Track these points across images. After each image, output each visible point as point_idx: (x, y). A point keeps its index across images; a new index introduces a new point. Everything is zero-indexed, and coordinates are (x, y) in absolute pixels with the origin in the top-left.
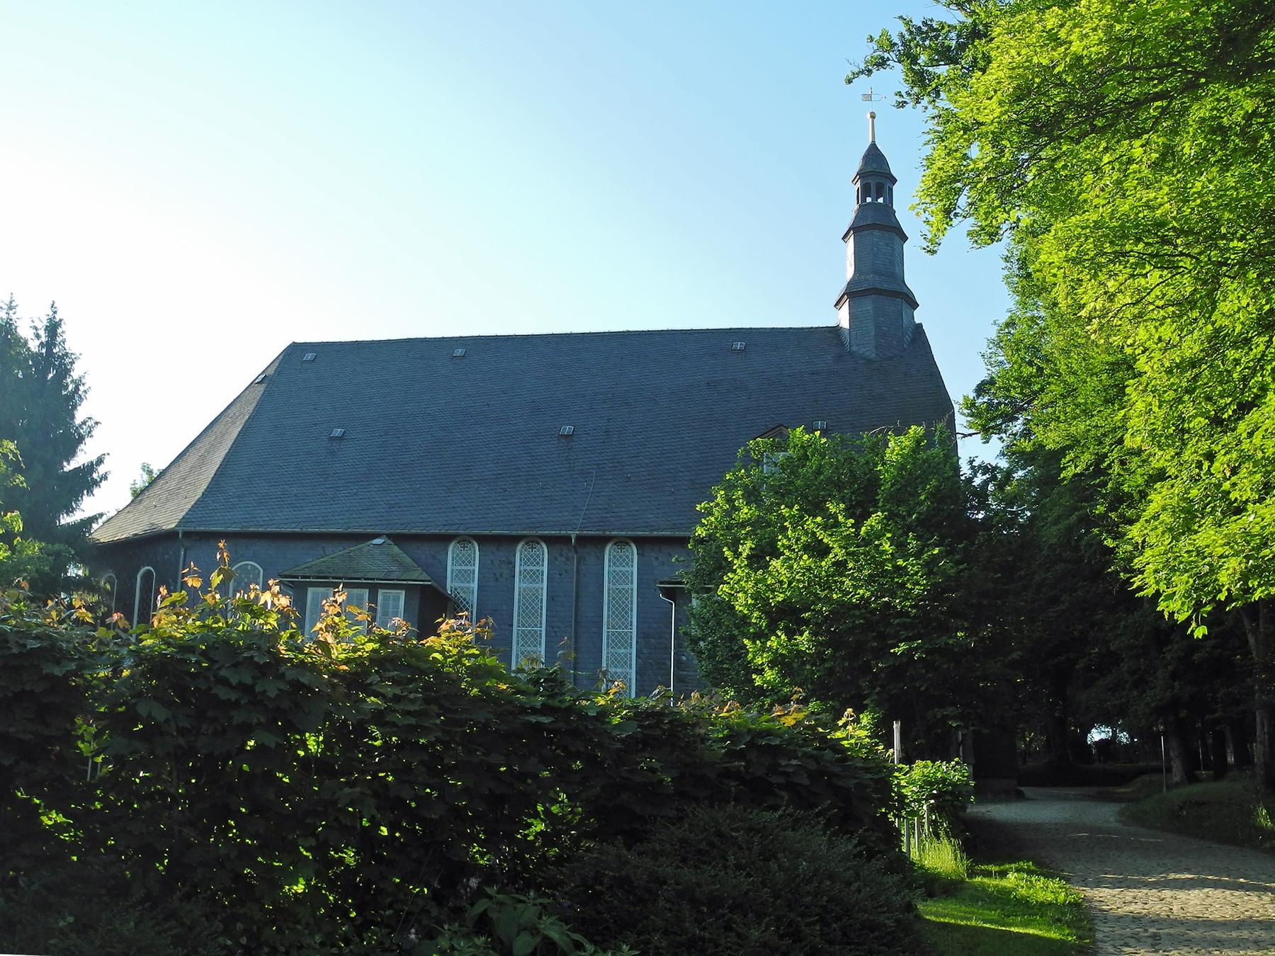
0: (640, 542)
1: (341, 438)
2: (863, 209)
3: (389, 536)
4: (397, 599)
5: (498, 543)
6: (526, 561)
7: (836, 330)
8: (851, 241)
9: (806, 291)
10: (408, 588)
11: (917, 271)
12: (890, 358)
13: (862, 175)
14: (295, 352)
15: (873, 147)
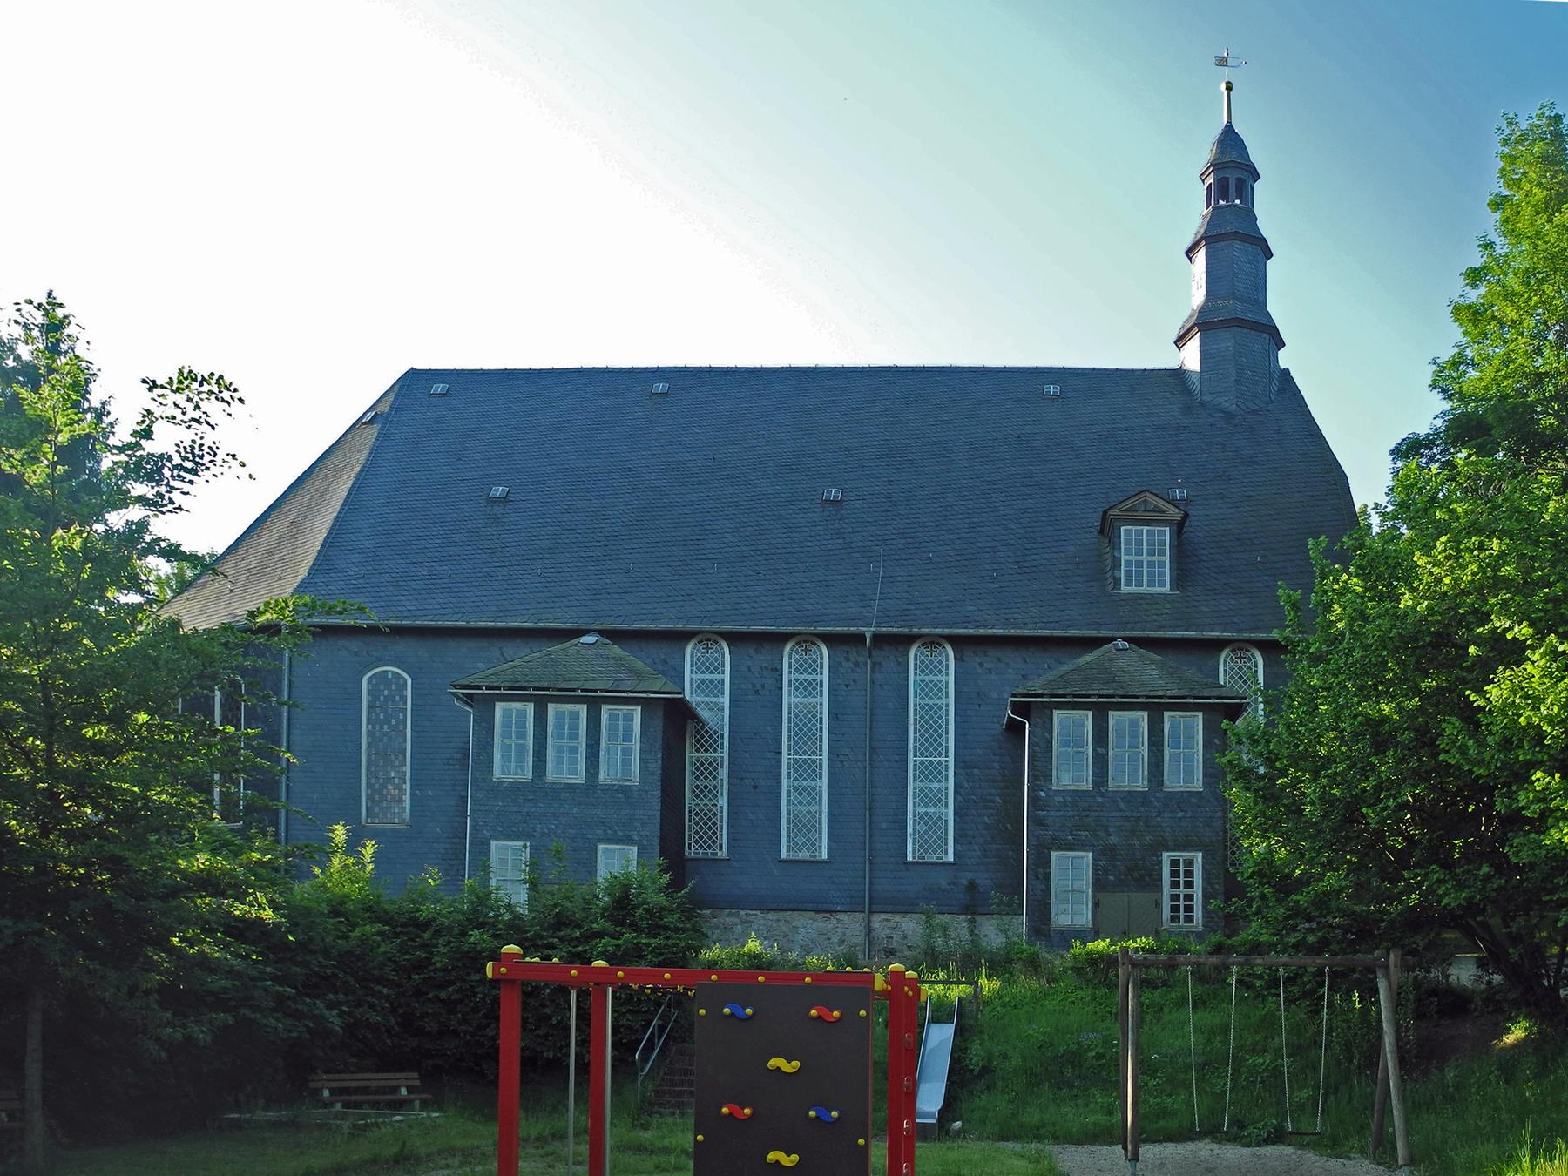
0: (957, 641)
1: (505, 500)
2: (1216, 216)
3: (601, 632)
4: (629, 718)
5: (874, 649)
6: (797, 668)
7: (1179, 374)
8: (1201, 256)
9: (1133, 317)
10: (645, 703)
11: (1283, 300)
12: (1254, 412)
13: (1216, 166)
14: (414, 381)
15: (1229, 128)
